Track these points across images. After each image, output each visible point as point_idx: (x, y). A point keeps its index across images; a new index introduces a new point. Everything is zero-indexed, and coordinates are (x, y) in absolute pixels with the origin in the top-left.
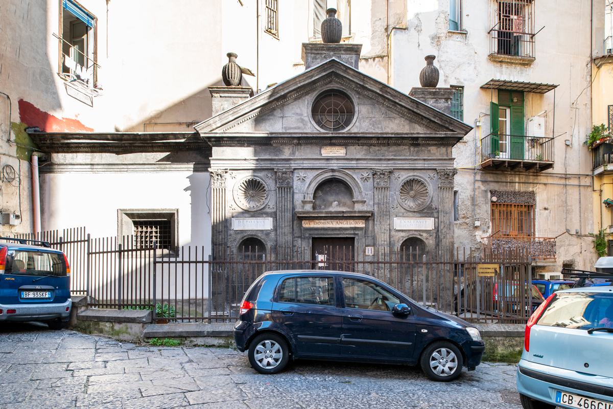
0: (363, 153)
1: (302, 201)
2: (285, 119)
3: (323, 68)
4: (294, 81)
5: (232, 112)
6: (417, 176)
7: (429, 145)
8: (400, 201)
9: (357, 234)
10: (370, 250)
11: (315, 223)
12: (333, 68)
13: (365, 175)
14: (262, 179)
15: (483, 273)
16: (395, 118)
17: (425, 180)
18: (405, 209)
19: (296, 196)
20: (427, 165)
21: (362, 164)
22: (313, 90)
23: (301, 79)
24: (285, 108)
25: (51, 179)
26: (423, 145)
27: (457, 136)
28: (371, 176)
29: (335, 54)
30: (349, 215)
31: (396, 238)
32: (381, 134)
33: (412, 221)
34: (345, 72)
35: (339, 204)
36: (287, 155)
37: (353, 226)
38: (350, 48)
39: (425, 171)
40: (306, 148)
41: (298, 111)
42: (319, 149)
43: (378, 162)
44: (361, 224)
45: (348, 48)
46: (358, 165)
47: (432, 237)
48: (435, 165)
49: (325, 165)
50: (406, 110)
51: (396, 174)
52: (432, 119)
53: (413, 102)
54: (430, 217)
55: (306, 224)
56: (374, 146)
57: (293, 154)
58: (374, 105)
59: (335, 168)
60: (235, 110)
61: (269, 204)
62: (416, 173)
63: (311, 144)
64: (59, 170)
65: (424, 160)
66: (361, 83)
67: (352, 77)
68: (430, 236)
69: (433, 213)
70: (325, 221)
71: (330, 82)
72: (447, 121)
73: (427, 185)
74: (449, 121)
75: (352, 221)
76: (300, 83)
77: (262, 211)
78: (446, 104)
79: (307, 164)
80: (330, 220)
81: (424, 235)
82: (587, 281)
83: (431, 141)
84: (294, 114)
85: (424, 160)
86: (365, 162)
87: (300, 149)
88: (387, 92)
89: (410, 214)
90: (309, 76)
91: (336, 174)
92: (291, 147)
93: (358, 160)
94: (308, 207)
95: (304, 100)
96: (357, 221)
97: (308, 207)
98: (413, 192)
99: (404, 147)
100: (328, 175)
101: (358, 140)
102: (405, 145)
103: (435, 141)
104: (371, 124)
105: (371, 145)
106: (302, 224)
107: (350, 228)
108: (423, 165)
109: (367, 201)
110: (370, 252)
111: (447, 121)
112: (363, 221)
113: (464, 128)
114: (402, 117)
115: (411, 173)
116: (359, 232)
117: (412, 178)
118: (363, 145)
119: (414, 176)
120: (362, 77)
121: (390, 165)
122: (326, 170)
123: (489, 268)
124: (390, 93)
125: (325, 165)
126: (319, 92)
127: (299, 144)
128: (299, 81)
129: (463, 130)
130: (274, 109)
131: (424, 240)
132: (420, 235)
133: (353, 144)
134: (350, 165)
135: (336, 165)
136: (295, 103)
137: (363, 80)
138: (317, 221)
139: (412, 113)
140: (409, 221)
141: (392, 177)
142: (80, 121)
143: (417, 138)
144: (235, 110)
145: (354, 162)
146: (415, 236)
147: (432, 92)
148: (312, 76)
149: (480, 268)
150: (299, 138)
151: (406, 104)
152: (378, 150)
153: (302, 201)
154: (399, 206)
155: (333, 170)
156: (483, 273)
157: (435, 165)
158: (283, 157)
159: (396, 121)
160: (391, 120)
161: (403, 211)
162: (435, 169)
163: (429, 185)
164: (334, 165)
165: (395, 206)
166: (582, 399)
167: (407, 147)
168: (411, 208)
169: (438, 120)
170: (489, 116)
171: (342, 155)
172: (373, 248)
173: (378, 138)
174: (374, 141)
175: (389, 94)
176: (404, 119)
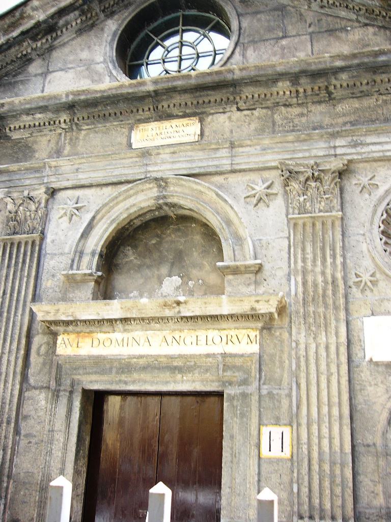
1: (67, 276)
2: (50, 77)
10: (276, 444)
11: (96, 342)
19: (49, 264)
24: (55, 54)
25: (108, 399)
28: (277, 188)
40: (27, 86)
42: (125, 131)
63: (105, 118)
82: (275, 460)
106: (55, 343)
110: (276, 444)
126: (134, 10)
130: (27, 60)
141: (352, 184)
142: (182, 353)
152: (302, 115)
159: (351, 37)
160: (338, 38)
165: (366, 278)
166: (43, 91)
172: (287, 430)
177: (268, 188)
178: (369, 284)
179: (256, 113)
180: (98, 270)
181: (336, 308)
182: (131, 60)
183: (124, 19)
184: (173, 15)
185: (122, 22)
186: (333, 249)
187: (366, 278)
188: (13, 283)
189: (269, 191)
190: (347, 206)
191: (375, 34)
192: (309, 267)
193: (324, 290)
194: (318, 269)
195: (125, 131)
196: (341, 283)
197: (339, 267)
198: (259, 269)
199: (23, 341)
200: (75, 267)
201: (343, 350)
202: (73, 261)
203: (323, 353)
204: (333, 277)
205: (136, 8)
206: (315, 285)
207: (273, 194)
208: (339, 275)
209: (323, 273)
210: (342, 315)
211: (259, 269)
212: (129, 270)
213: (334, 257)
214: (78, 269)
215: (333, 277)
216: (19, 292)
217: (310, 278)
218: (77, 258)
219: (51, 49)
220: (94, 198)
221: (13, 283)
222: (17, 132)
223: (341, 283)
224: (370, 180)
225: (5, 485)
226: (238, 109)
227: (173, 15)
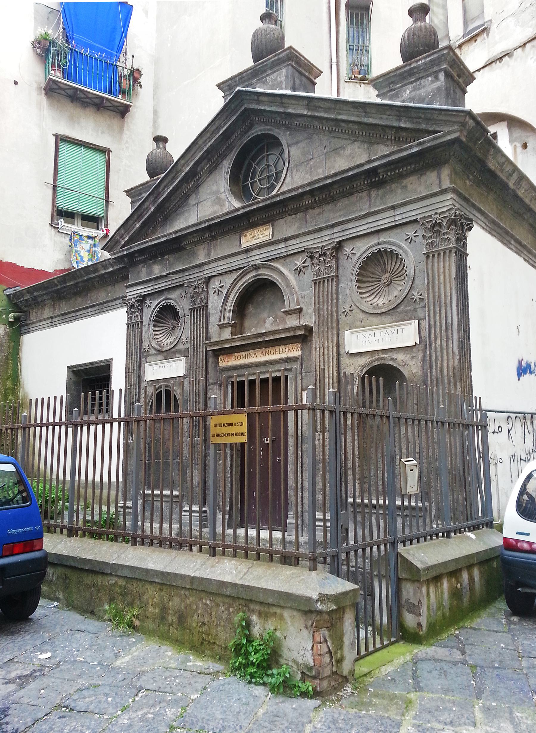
0: (296, 226)
1: (218, 325)
2: (200, 205)
3: (230, 110)
4: (197, 146)
5: (135, 217)
6: (384, 243)
7: (402, 176)
8: (356, 297)
9: (290, 370)
11: (234, 358)
12: (244, 104)
13: (299, 263)
14: (176, 302)
15: (218, 435)
16: (343, 148)
17: (400, 247)
18: (363, 311)
20: (399, 216)
21: (295, 245)
22: (230, 149)
23: (204, 139)
24: (201, 189)
26: (392, 180)
27: (444, 139)
29: (258, 80)
30: (272, 338)
31: (349, 370)
32: (309, 184)
33: (378, 332)
34: (258, 102)
35: (275, 321)
36: (202, 259)
37: (284, 356)
38: (275, 60)
39: (396, 231)
41: (214, 188)
42: (238, 237)
43: (316, 235)
44: (295, 352)
45: (273, 62)
46: (289, 248)
47: (415, 360)
48: (414, 213)
49: (243, 261)
50: (356, 127)
51: (347, 249)
52: (396, 124)
53: (357, 108)
54: (411, 319)
55: (224, 362)
56: (311, 208)
57: (209, 254)
58: (310, 137)
59: (257, 262)
60: (139, 213)
61: (182, 337)
62: (383, 238)
64: (32, 329)
65: (393, 208)
66: (282, 110)
67: (269, 106)
68: (413, 357)
69: (415, 310)
70: (246, 353)
71: (251, 127)
72: (420, 118)
73: (404, 256)
74: (423, 116)
75: (282, 348)
76: (205, 146)
77: (176, 348)
78: (437, 84)
79: (223, 266)
80: (252, 351)
81: (400, 357)
83: (402, 167)
84: (209, 194)
85: (393, 208)
86: (297, 241)
87: (216, 245)
88: (316, 108)
89: (375, 320)
90: (215, 130)
91: (261, 272)
92: (205, 245)
93: (286, 240)
94: (227, 334)
95: (222, 168)
96: (290, 346)
97: (227, 334)
98: (387, 275)
99: (361, 194)
100: (249, 277)
101: (285, 206)
102: (362, 191)
103: (410, 164)
104: (307, 173)
105: (307, 209)
107: (280, 359)
108: (392, 219)
109: (304, 309)
111: (420, 118)
112: (299, 345)
113: (454, 119)
114: (355, 141)
115: (374, 240)
116: (295, 366)
117: (375, 249)
118: (295, 212)
119: (379, 244)
120: (278, 98)
121: (337, 235)
122: (243, 271)
123: (229, 425)
124: (321, 108)
125: (243, 261)
126: (237, 150)
127: (214, 238)
128: (204, 143)
129: (454, 122)
131: (400, 368)
132: (392, 359)
133: (282, 215)
134: (277, 252)
135: (257, 257)
136: (211, 177)
137: (282, 103)
138: (236, 354)
139: (367, 127)
140: (372, 333)
143: (374, 171)
144: (139, 213)
145: (282, 245)
146: (382, 362)
147: (405, 72)
148: (218, 129)
149: (216, 425)
150: (209, 228)
151: (348, 115)
153: (218, 325)
154: (355, 307)
155: (256, 267)
156: (218, 435)
157: (414, 213)
158: (198, 262)
159: (346, 152)
161: (361, 316)
162: (416, 221)
163: (407, 255)
164: (256, 258)
167: (365, 194)
168: (374, 308)
169: (405, 122)
170: (472, 70)
171: (268, 238)
173: (311, 192)
174: (308, 201)
175: (320, 110)
176: (359, 143)
177: (304, 263)
178: (349, 312)
179: (298, 215)
180: (232, 320)
181: (332, 328)
182: (243, 183)
183: (232, 159)
184: (261, 145)
185: (231, 162)
186: (332, 296)
187: (347, 308)
188: (197, 332)
189: (305, 265)
190: (340, 269)
191: (359, 148)
192: (321, 307)
193: (328, 320)
194: (325, 308)
195: (238, 237)
196: (335, 314)
197: (334, 305)
198: (300, 310)
199: (335, 358)
200: (222, 320)
201: (335, 349)
202: (221, 317)
203: (326, 350)
204: (332, 311)
205: (237, 150)
206: (324, 316)
207: (306, 266)
208: (334, 309)
209: (327, 309)
210: (335, 332)
211: (300, 310)
212: (251, 316)
213: (332, 301)
214: (224, 321)
215: (332, 311)
216: (200, 336)
217: (322, 313)
218: (223, 315)
219: (198, 186)
220: (229, 280)
221: (197, 332)
222: (188, 246)
223: (335, 314)
224: (352, 250)
225: (328, 534)
226: (289, 215)
227: (261, 145)
